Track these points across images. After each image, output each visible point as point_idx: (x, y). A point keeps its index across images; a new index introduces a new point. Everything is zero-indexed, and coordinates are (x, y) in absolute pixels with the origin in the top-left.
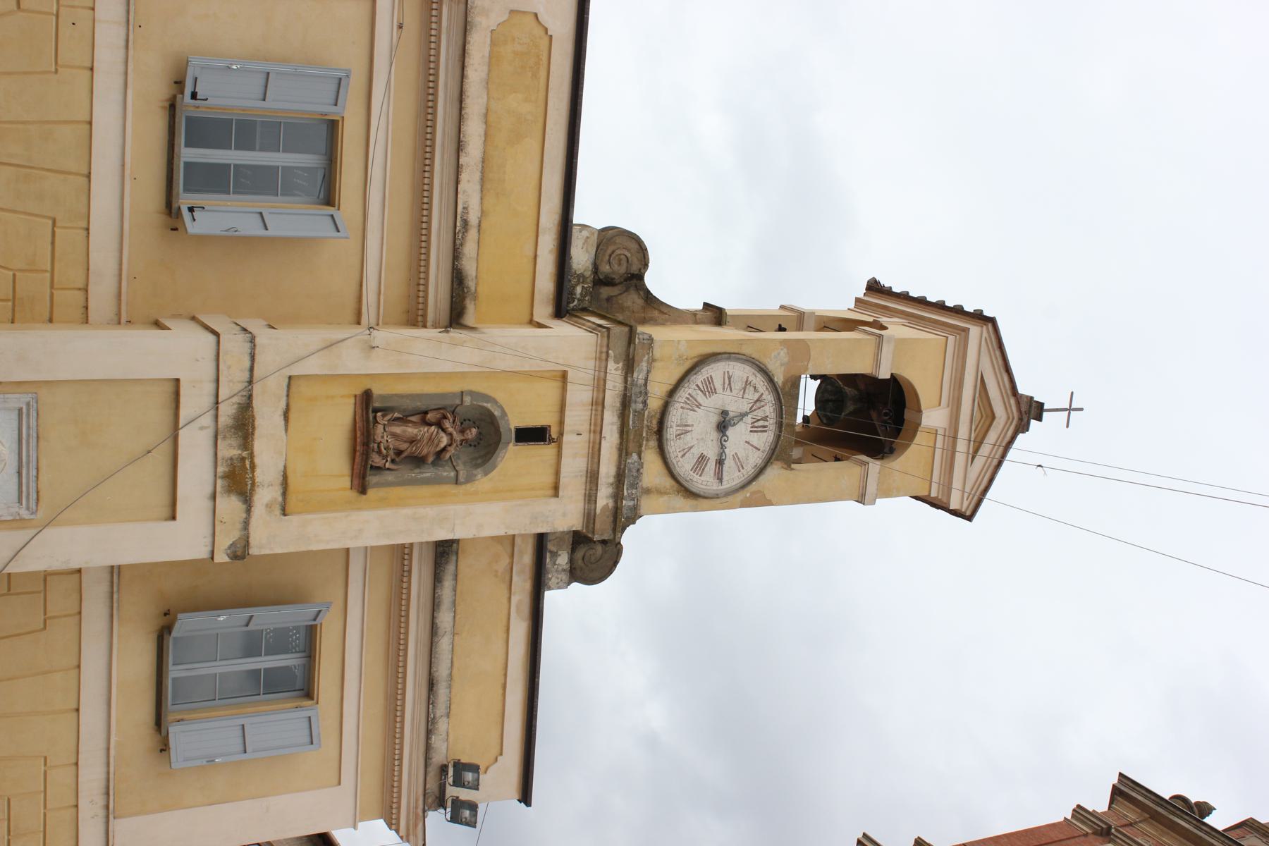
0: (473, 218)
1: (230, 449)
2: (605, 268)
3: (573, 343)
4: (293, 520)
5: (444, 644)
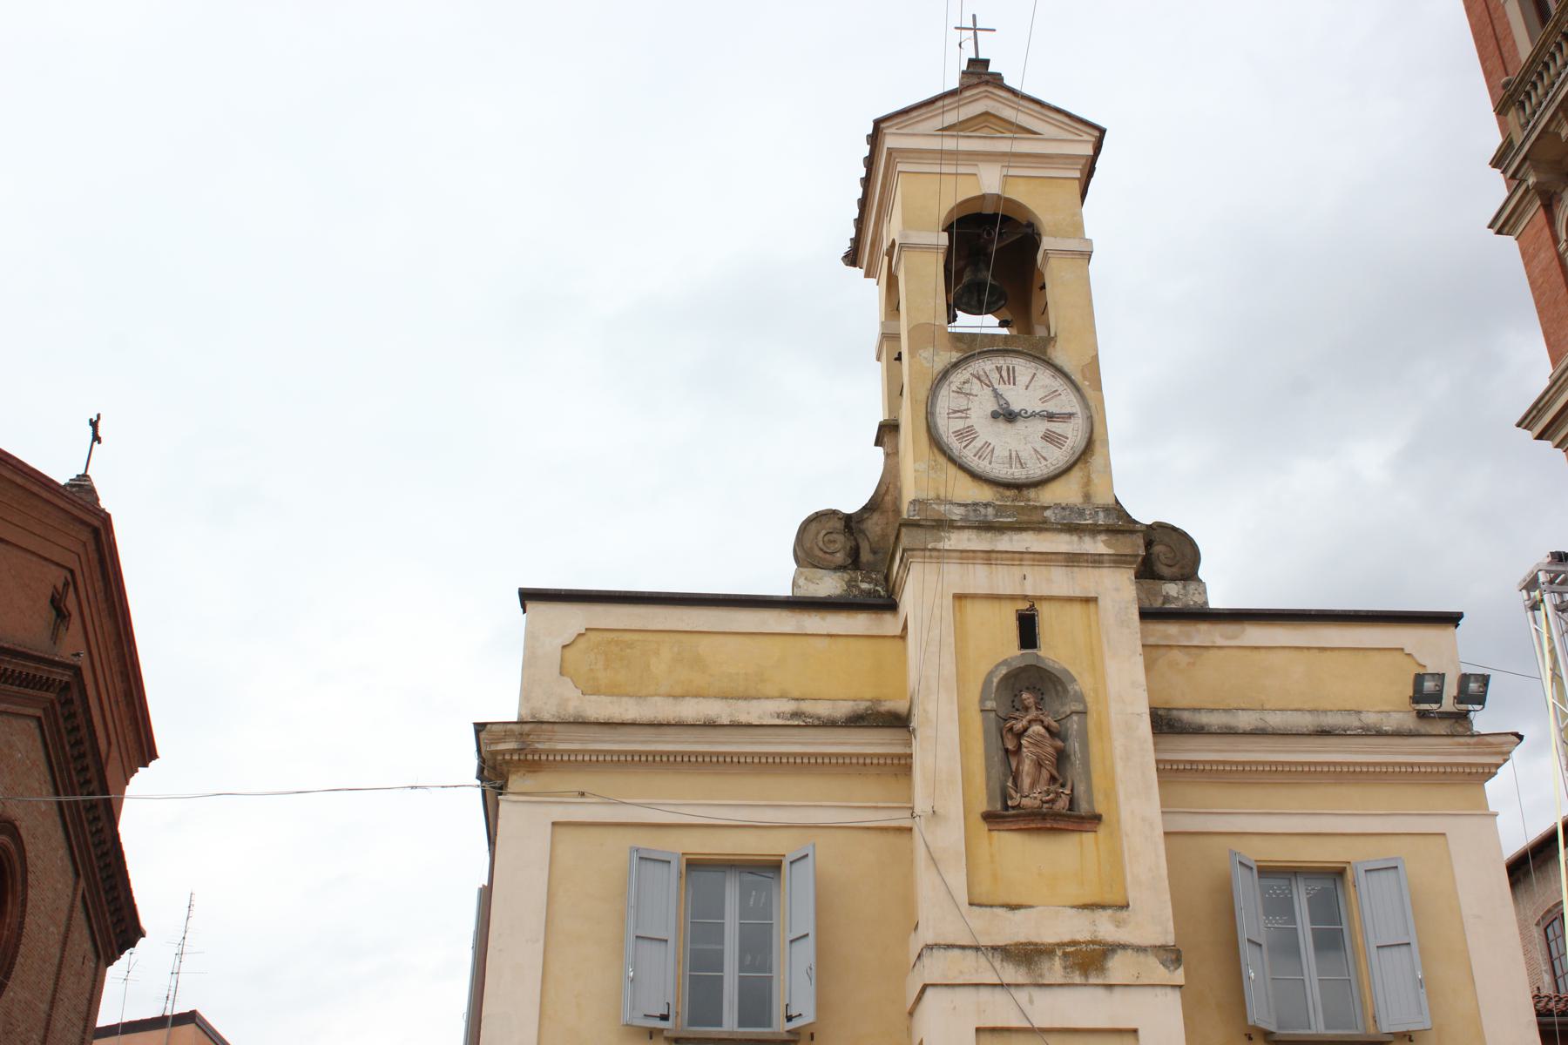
0: (789, 707)
1: (1055, 970)
2: (840, 557)
3: (922, 589)
5: (1275, 720)
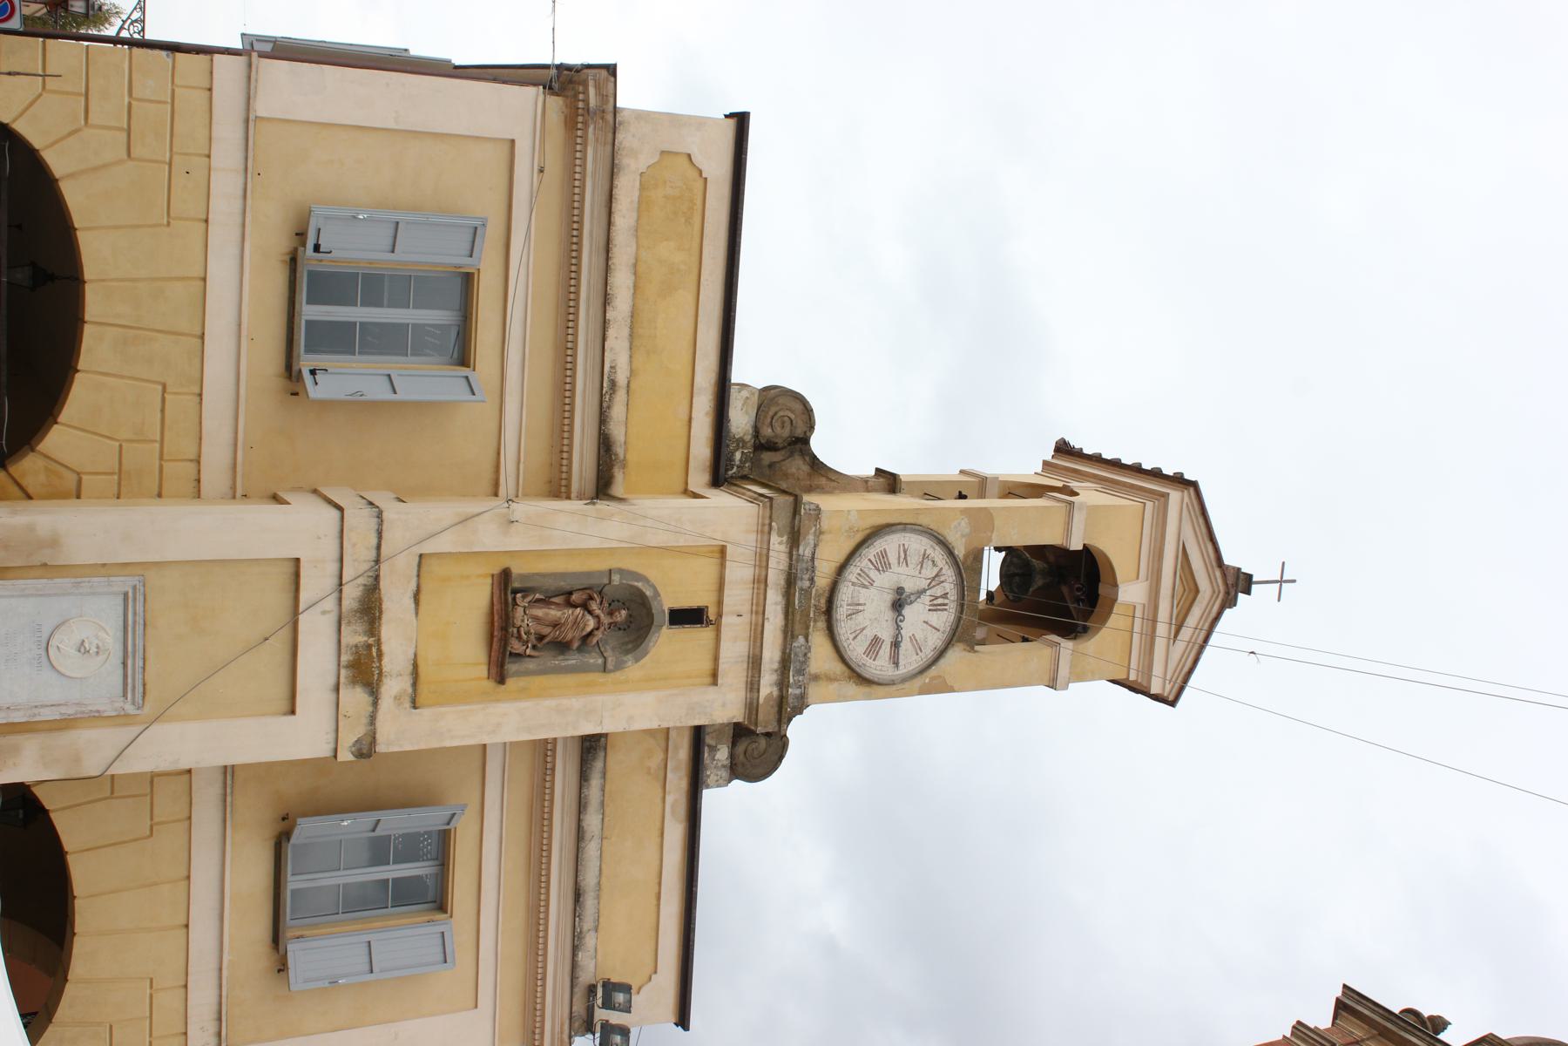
0: (621, 379)
1: (354, 636)
2: (767, 432)
3: (731, 515)
4: (425, 713)
